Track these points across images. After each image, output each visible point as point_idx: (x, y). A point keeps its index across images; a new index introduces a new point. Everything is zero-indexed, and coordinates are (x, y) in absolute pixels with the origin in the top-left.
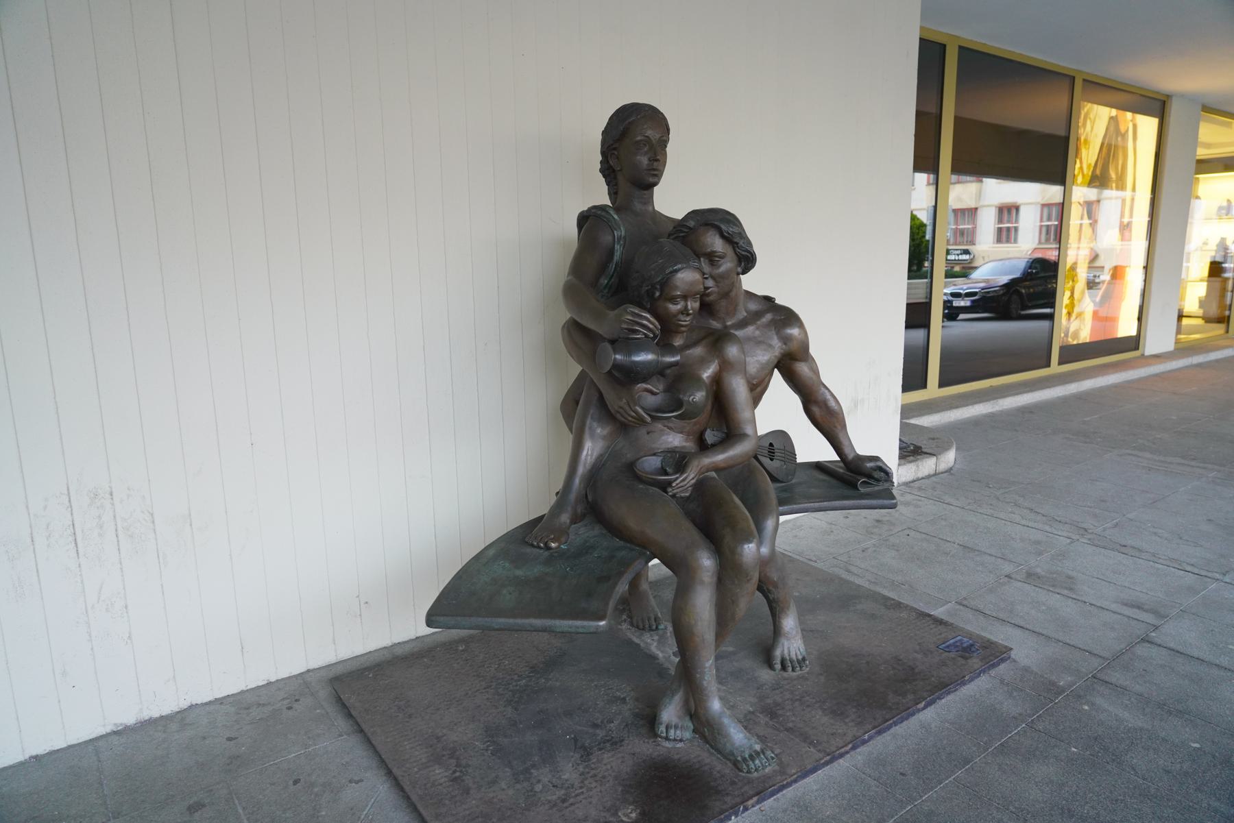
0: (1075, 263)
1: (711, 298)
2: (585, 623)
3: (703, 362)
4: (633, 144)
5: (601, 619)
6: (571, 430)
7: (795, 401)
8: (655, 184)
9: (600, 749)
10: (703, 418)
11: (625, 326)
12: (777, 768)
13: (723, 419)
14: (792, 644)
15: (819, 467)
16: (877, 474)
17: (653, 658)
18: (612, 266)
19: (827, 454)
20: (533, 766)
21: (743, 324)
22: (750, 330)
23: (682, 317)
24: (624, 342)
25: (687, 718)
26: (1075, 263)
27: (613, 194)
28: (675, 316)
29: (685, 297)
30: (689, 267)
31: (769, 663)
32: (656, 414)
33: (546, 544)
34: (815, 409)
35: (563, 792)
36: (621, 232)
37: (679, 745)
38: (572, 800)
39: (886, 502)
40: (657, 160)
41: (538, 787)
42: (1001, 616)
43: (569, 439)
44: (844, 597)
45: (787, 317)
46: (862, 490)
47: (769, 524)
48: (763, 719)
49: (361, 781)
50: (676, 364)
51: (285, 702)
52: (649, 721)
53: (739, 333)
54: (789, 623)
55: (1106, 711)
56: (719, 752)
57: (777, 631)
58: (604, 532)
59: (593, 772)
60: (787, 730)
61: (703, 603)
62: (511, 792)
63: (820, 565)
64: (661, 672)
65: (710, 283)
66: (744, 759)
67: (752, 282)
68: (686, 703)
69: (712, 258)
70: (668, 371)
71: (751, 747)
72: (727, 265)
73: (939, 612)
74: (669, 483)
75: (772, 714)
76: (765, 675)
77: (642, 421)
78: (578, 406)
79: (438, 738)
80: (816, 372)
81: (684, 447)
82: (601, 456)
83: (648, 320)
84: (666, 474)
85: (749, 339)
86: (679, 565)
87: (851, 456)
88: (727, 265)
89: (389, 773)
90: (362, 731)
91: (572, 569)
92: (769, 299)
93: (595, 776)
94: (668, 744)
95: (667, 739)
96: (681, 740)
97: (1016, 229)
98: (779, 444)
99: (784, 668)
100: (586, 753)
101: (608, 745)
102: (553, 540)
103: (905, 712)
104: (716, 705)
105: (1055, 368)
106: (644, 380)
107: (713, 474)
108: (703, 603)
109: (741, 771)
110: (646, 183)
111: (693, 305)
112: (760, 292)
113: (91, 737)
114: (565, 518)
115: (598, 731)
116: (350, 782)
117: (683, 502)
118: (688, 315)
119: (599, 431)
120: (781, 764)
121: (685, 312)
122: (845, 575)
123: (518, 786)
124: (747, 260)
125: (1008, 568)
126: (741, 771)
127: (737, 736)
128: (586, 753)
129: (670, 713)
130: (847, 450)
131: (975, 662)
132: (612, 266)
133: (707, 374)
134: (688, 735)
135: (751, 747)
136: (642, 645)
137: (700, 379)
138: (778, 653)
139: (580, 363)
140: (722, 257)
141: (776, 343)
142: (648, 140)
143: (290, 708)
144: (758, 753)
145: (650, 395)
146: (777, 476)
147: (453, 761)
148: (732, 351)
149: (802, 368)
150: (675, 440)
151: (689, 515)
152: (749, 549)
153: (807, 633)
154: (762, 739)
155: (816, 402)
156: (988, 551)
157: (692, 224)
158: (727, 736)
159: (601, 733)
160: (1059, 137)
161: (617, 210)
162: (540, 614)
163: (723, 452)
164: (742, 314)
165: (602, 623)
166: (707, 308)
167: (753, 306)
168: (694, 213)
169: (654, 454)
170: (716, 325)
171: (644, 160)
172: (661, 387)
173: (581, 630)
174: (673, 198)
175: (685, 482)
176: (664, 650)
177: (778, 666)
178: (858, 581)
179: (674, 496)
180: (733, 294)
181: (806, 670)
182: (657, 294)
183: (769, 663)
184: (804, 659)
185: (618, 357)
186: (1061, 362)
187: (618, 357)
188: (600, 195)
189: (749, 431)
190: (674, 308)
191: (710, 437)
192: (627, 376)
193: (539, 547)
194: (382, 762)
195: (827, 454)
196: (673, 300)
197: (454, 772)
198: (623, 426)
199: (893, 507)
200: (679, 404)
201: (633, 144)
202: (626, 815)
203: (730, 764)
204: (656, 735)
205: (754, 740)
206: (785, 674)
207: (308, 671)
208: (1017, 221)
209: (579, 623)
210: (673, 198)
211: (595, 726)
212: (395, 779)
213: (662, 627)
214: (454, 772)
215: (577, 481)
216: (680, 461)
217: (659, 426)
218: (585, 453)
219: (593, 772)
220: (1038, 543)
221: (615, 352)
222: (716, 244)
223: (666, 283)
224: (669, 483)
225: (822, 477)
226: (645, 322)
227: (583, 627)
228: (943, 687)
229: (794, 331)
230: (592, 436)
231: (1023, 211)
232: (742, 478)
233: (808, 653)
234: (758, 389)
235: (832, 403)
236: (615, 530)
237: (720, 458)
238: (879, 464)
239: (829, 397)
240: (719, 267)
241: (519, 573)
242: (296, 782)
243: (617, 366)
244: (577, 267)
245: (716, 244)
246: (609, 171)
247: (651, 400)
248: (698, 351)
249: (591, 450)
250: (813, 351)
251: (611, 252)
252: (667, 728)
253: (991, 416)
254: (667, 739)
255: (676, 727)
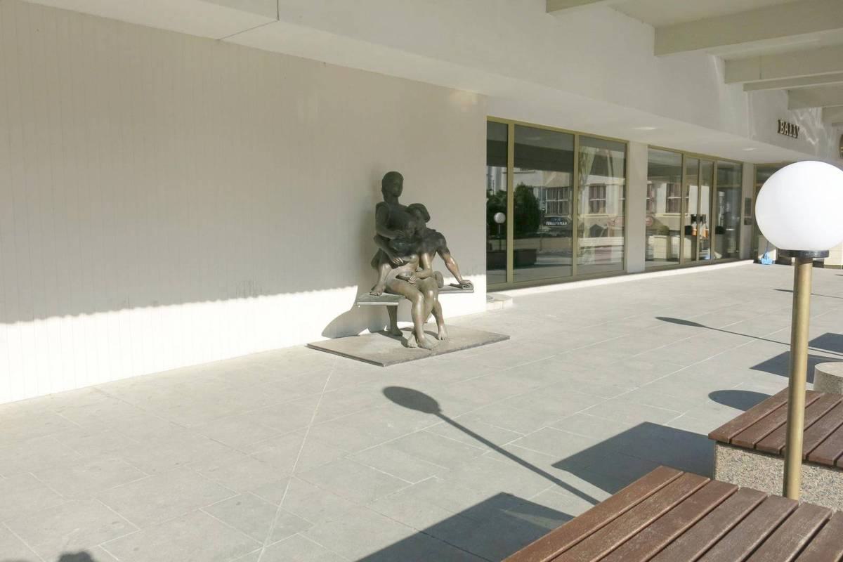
0: (761, 263)
4: (392, 183)
26: (761, 263)
55: (19, 535)
67: (429, 225)
97: (604, 202)
113: (530, 471)
124: (427, 218)
160: (676, 168)
168: (412, 205)
174: (405, 200)
208: (604, 196)
210: (405, 200)
222: (418, 213)
231: (609, 190)
246: (384, 190)
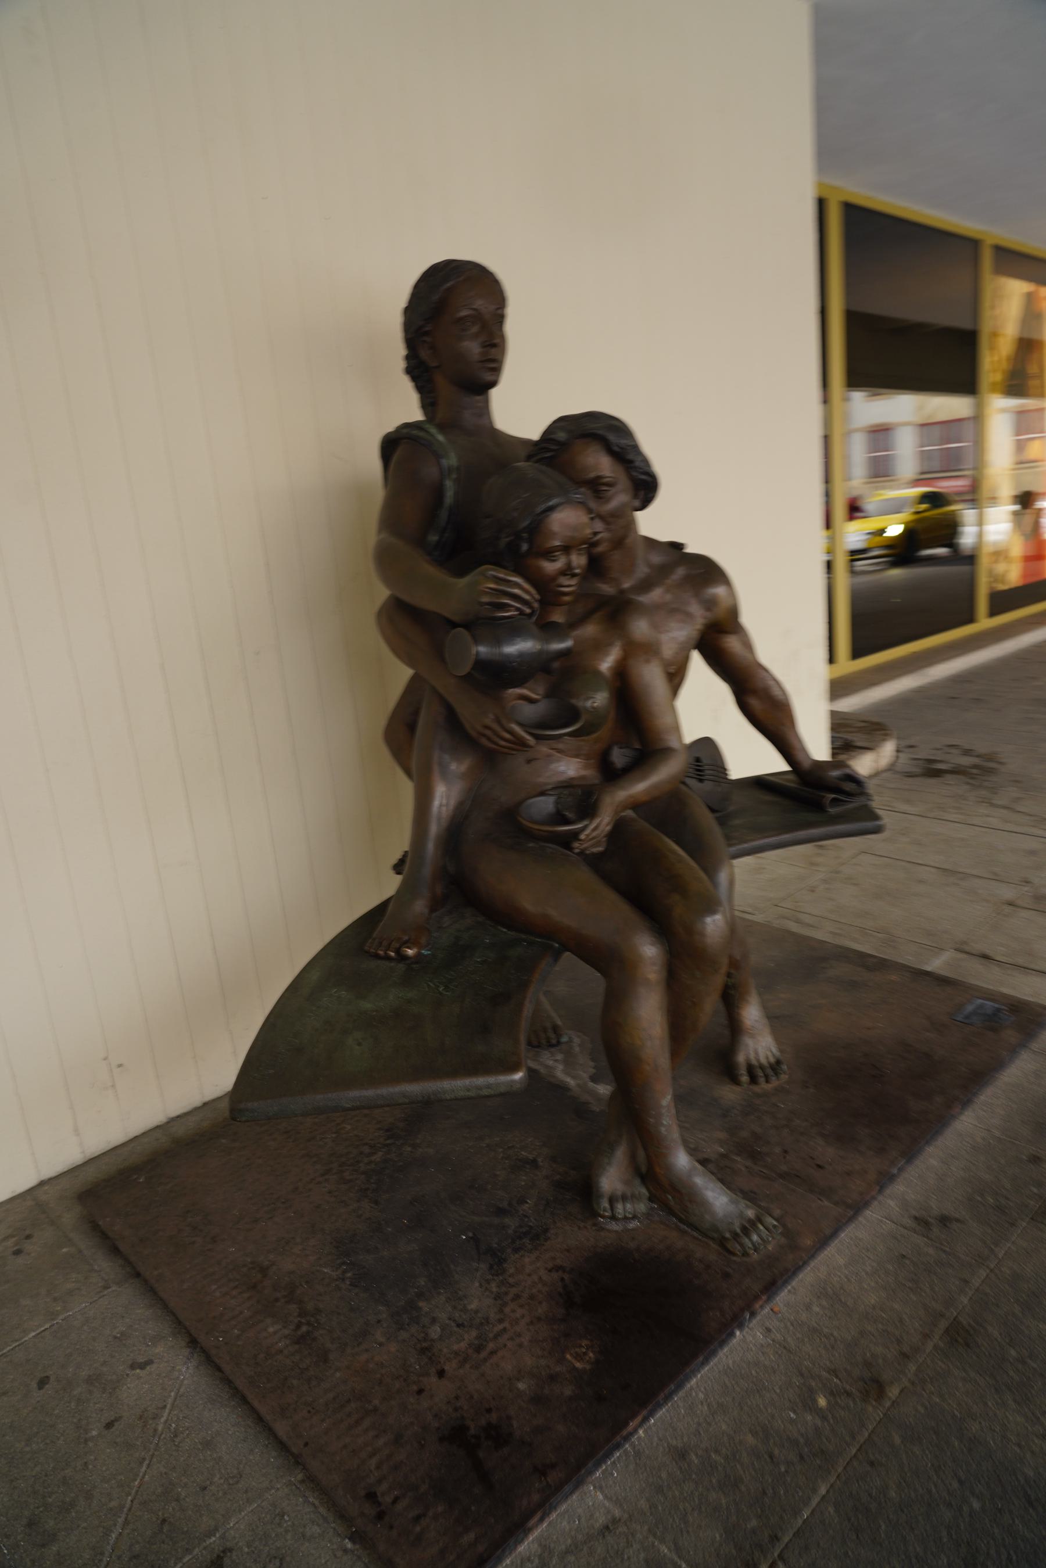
1: (600, 549)
2: (491, 1080)
3: (599, 647)
4: (453, 322)
5: (514, 1069)
6: (408, 773)
7: (721, 691)
8: (493, 384)
9: (516, 1250)
10: (604, 733)
11: (485, 599)
12: (783, 1240)
13: (634, 729)
14: (760, 1044)
15: (760, 783)
16: (849, 786)
17: (561, 1088)
18: (443, 515)
19: (769, 762)
20: (420, 1295)
21: (646, 585)
22: (656, 595)
23: (564, 581)
24: (486, 623)
25: (637, 1182)
27: (428, 404)
28: (553, 578)
29: (566, 549)
30: (569, 502)
31: (730, 1073)
32: (541, 727)
33: (398, 951)
34: (754, 703)
35: (474, 1333)
36: (452, 460)
37: (633, 1225)
38: (491, 1346)
39: (869, 824)
40: (494, 345)
41: (435, 1331)
42: (1020, 961)
43: (407, 789)
44: (811, 961)
45: (705, 572)
46: (832, 811)
47: (723, 877)
48: (740, 1162)
49: (150, 1362)
50: (566, 653)
51: (10, 1242)
52: (585, 1193)
53: (646, 599)
54: (752, 1013)
56: (696, 1228)
57: (735, 1028)
58: (481, 919)
59: (513, 1291)
60: (783, 1176)
61: (649, 1014)
62: (393, 1347)
63: (758, 918)
64: (580, 1110)
65: (599, 526)
66: (735, 1236)
67: (652, 523)
68: (633, 1157)
69: (597, 487)
70: (556, 665)
71: (741, 1215)
72: (620, 498)
73: (936, 964)
74: (575, 835)
75: (754, 1156)
76: (729, 1094)
77: (522, 744)
78: (409, 733)
79: (264, 1271)
80: (748, 645)
81: (582, 778)
82: (460, 804)
83: (520, 586)
84: (567, 822)
85: (658, 607)
86: (610, 963)
87: (806, 765)
88: (620, 498)
89: (193, 1343)
90: (138, 1275)
91: (447, 988)
92: (677, 547)
93: (517, 1297)
94: (614, 1226)
95: (613, 1217)
96: (635, 1217)
98: (706, 756)
99: (753, 1080)
100: (497, 1262)
101: (526, 1241)
102: (407, 944)
103: (933, 1125)
104: (682, 1160)
105: (984, 623)
106: (521, 683)
107: (629, 813)
108: (649, 1014)
109: (734, 1254)
110: (479, 376)
111: (579, 560)
112: (664, 537)
114: (420, 906)
115: (507, 1221)
116: (133, 1367)
117: (594, 862)
118: (574, 575)
119: (453, 766)
120: (787, 1233)
121: (567, 571)
122: (794, 927)
123: (404, 1335)
124: (645, 488)
125: (1007, 893)
126: (734, 1254)
127: (718, 1200)
128: (497, 1262)
129: (611, 1179)
130: (800, 757)
131: (1010, 1035)
132: (443, 515)
133: (606, 664)
134: (642, 1207)
135: (741, 1215)
136: (542, 1071)
137: (598, 673)
138: (741, 1058)
139: (410, 663)
140: (610, 485)
141: (696, 609)
142: (477, 317)
143: (18, 1252)
144: (752, 1223)
145: (527, 702)
146: (708, 808)
147: (293, 1307)
148: (641, 627)
149: (732, 643)
150: (569, 768)
151: (607, 878)
152: (714, 925)
153: (774, 1019)
154: (749, 1196)
155: (755, 692)
156: (975, 872)
157: (561, 436)
158: (704, 1204)
159: (511, 1223)
161: (442, 427)
162: (417, 1074)
163: (643, 778)
164: (642, 571)
165: (518, 1076)
166: (596, 567)
167: (656, 559)
169: (543, 793)
170: (607, 589)
171: (473, 348)
172: (541, 690)
173: (485, 1092)
174: (521, 407)
175: (596, 829)
176: (578, 1073)
177: (745, 1079)
178: (819, 935)
179: (582, 853)
180: (628, 541)
181: (784, 1077)
182: (525, 547)
183: (730, 1073)
184: (778, 1062)
185: (482, 649)
186: (993, 612)
187: (482, 649)
188: (407, 407)
189: (674, 744)
190: (550, 567)
191: (619, 757)
192: (497, 676)
193: (388, 958)
194: (179, 1326)
195: (769, 762)
196: (549, 554)
197: (299, 1326)
198: (489, 756)
199: (877, 830)
200: (571, 715)
201: (453, 322)
202: (579, 1357)
203: (714, 1246)
204: (595, 1214)
205: (743, 1203)
206: (756, 1089)
207: (42, 1183)
209: (480, 1081)
210: (521, 407)
211: (501, 1212)
212: (204, 1351)
213: (564, 1039)
214: (299, 1326)
215: (431, 846)
216: (582, 801)
217: (544, 749)
218: (436, 803)
219: (513, 1291)
220: (1033, 853)
221: (477, 641)
222: (602, 464)
223: (536, 528)
224: (575, 835)
225: (768, 797)
226: (516, 591)
227: (489, 1086)
228: (977, 1078)
229: (720, 591)
230: (445, 775)
232: (667, 812)
233: (781, 1051)
234: (676, 677)
235: (776, 692)
236: (499, 915)
237: (640, 787)
238: (847, 771)
239: (771, 683)
240: (608, 500)
241: (367, 1005)
242: (42, 1383)
243: (482, 665)
244: (392, 519)
245: (602, 464)
246: (419, 370)
247: (529, 712)
248: (590, 630)
249: (444, 796)
250: (747, 619)
251: (439, 492)
252: (612, 1200)
253: (920, 691)
254: (613, 1217)
255: (624, 1198)
